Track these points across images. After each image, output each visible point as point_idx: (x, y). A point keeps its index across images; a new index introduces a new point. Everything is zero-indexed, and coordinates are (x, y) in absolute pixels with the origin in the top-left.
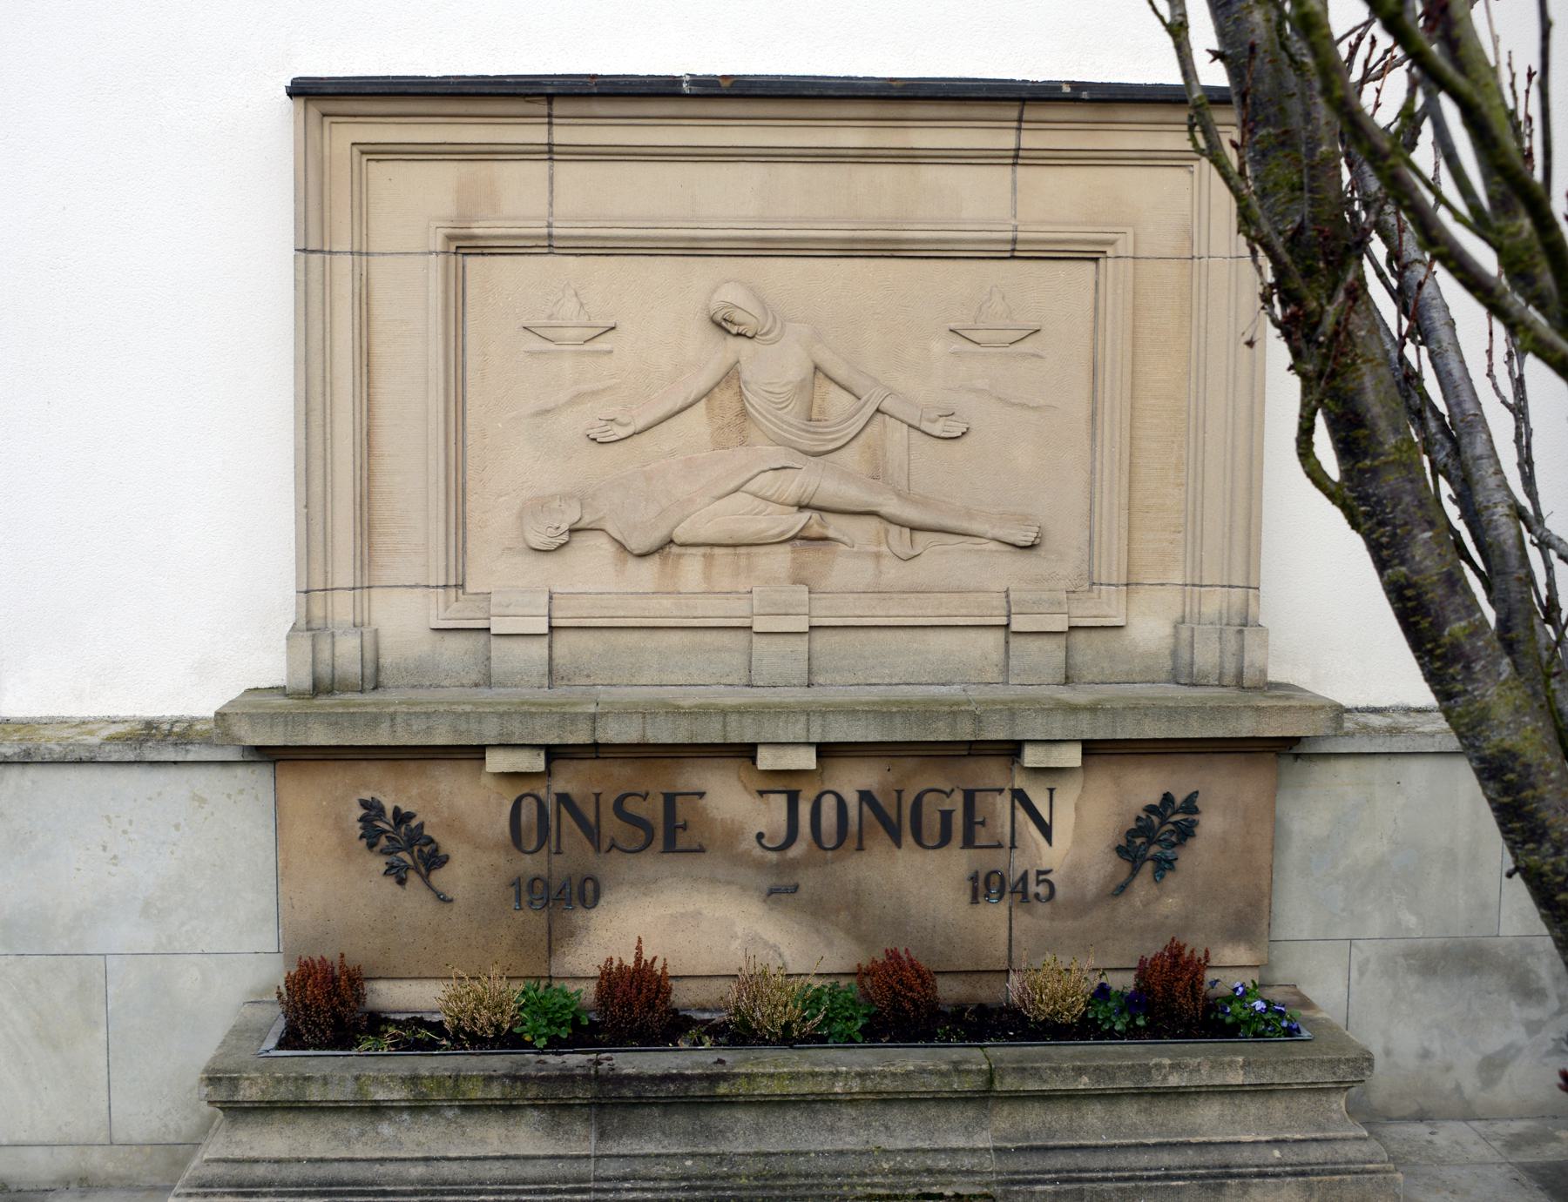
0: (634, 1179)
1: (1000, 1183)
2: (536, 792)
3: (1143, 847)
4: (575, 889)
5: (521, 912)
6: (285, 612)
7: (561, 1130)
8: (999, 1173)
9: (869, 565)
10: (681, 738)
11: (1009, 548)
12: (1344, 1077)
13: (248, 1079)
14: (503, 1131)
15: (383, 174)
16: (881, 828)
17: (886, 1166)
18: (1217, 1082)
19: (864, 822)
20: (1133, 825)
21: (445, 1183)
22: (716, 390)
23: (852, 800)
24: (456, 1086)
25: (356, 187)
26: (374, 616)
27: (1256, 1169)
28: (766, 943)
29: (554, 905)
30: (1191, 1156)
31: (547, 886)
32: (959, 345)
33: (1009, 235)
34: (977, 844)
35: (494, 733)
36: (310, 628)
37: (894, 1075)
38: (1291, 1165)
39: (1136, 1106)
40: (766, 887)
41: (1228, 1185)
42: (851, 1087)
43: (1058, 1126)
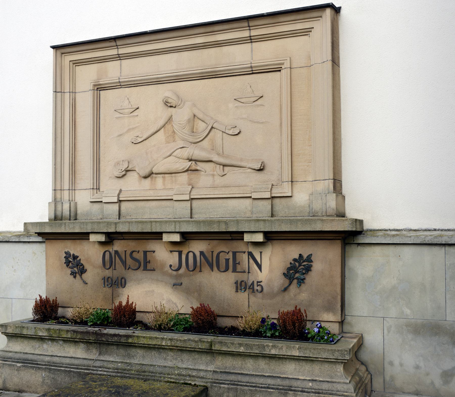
0: (103, 368)
1: (211, 382)
2: (109, 250)
3: (293, 274)
4: (119, 282)
5: (105, 288)
7: (89, 351)
8: (212, 379)
9: (211, 178)
10: (139, 230)
11: (254, 171)
12: (337, 357)
13: (9, 326)
14: (74, 350)
16: (207, 264)
17: (176, 372)
18: (289, 354)
19: (202, 262)
20: (289, 266)
21: (53, 363)
22: (166, 125)
23: (198, 254)
24: (59, 333)
25: (71, 73)
26: (76, 198)
27: (301, 389)
28: (173, 302)
29: (114, 286)
30: (279, 381)
31: (112, 280)
32: (237, 104)
33: (249, 65)
34: (237, 271)
35: (90, 229)
37: (180, 340)
38: (315, 389)
39: (264, 362)
40: (172, 283)
41: (289, 393)
42: (168, 344)
43: (237, 366)
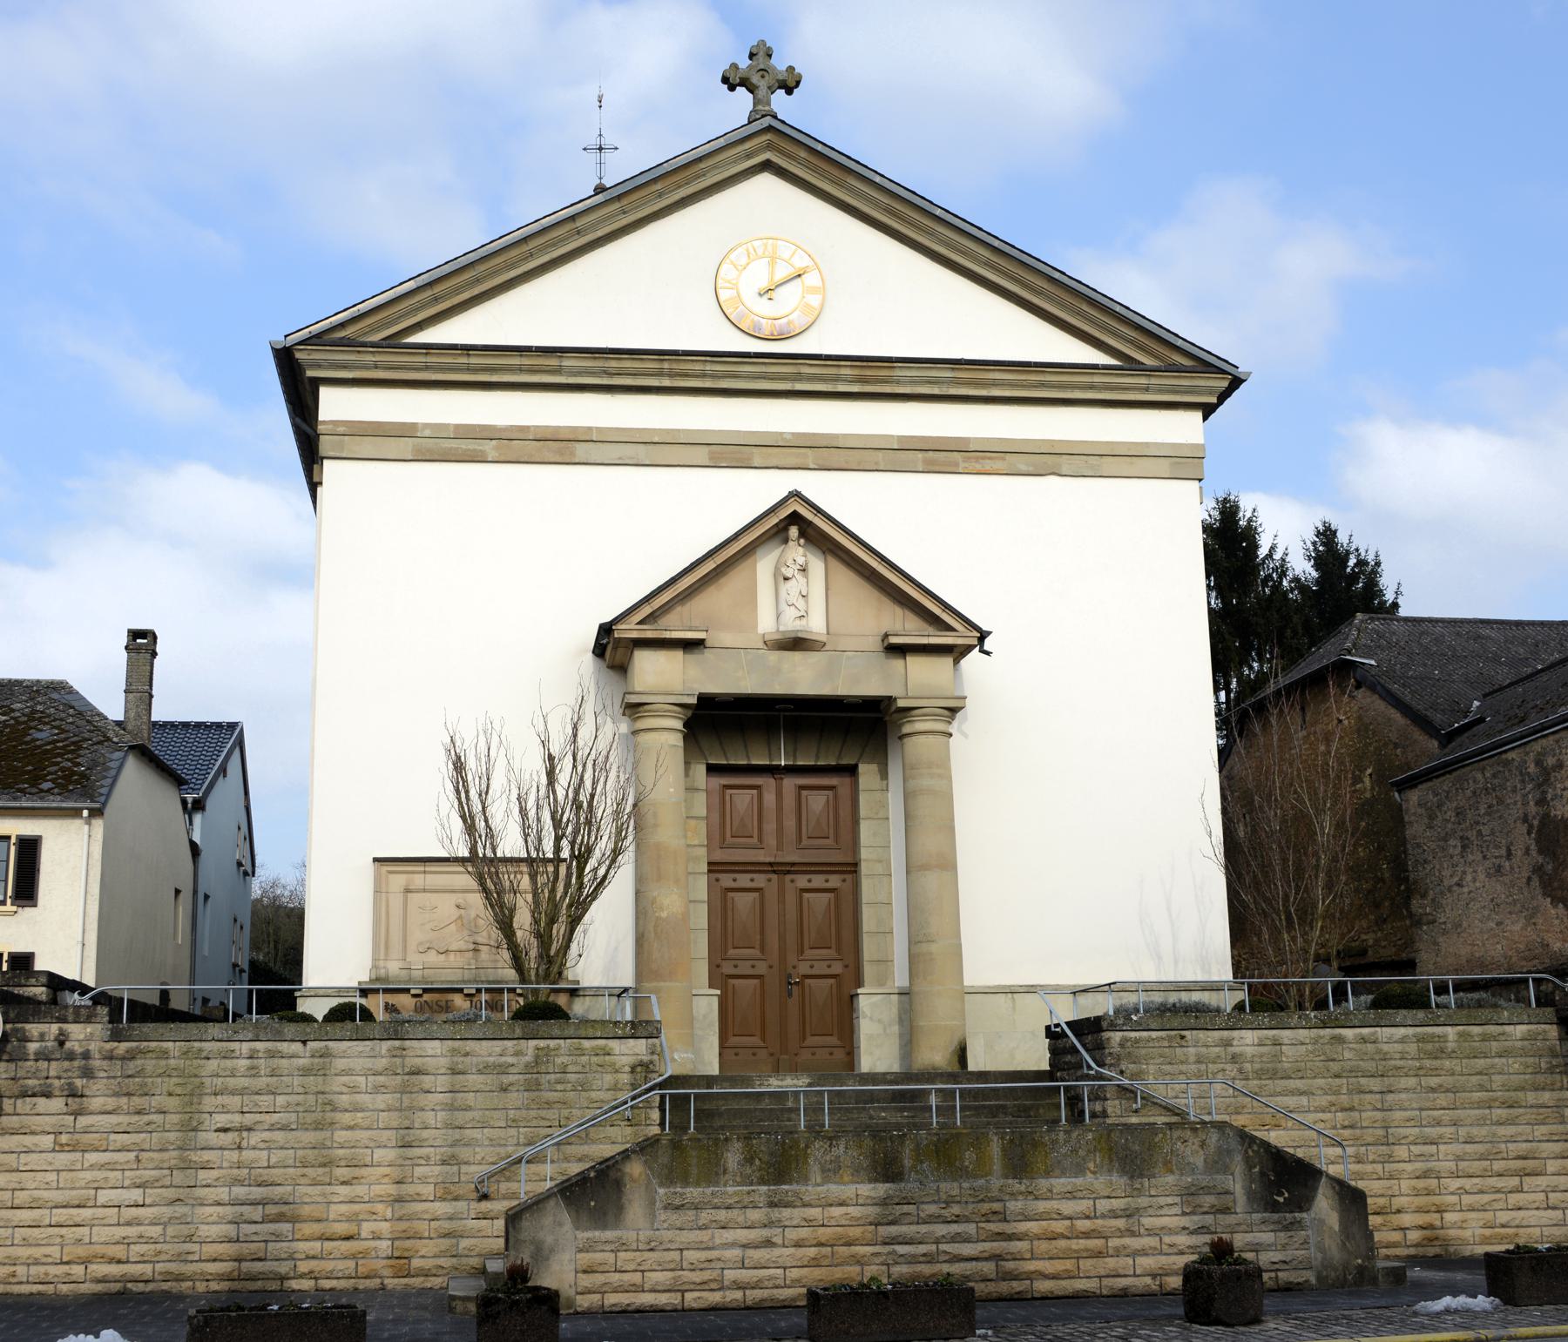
6: (369, 964)
15: (392, 876)
36: (375, 967)
